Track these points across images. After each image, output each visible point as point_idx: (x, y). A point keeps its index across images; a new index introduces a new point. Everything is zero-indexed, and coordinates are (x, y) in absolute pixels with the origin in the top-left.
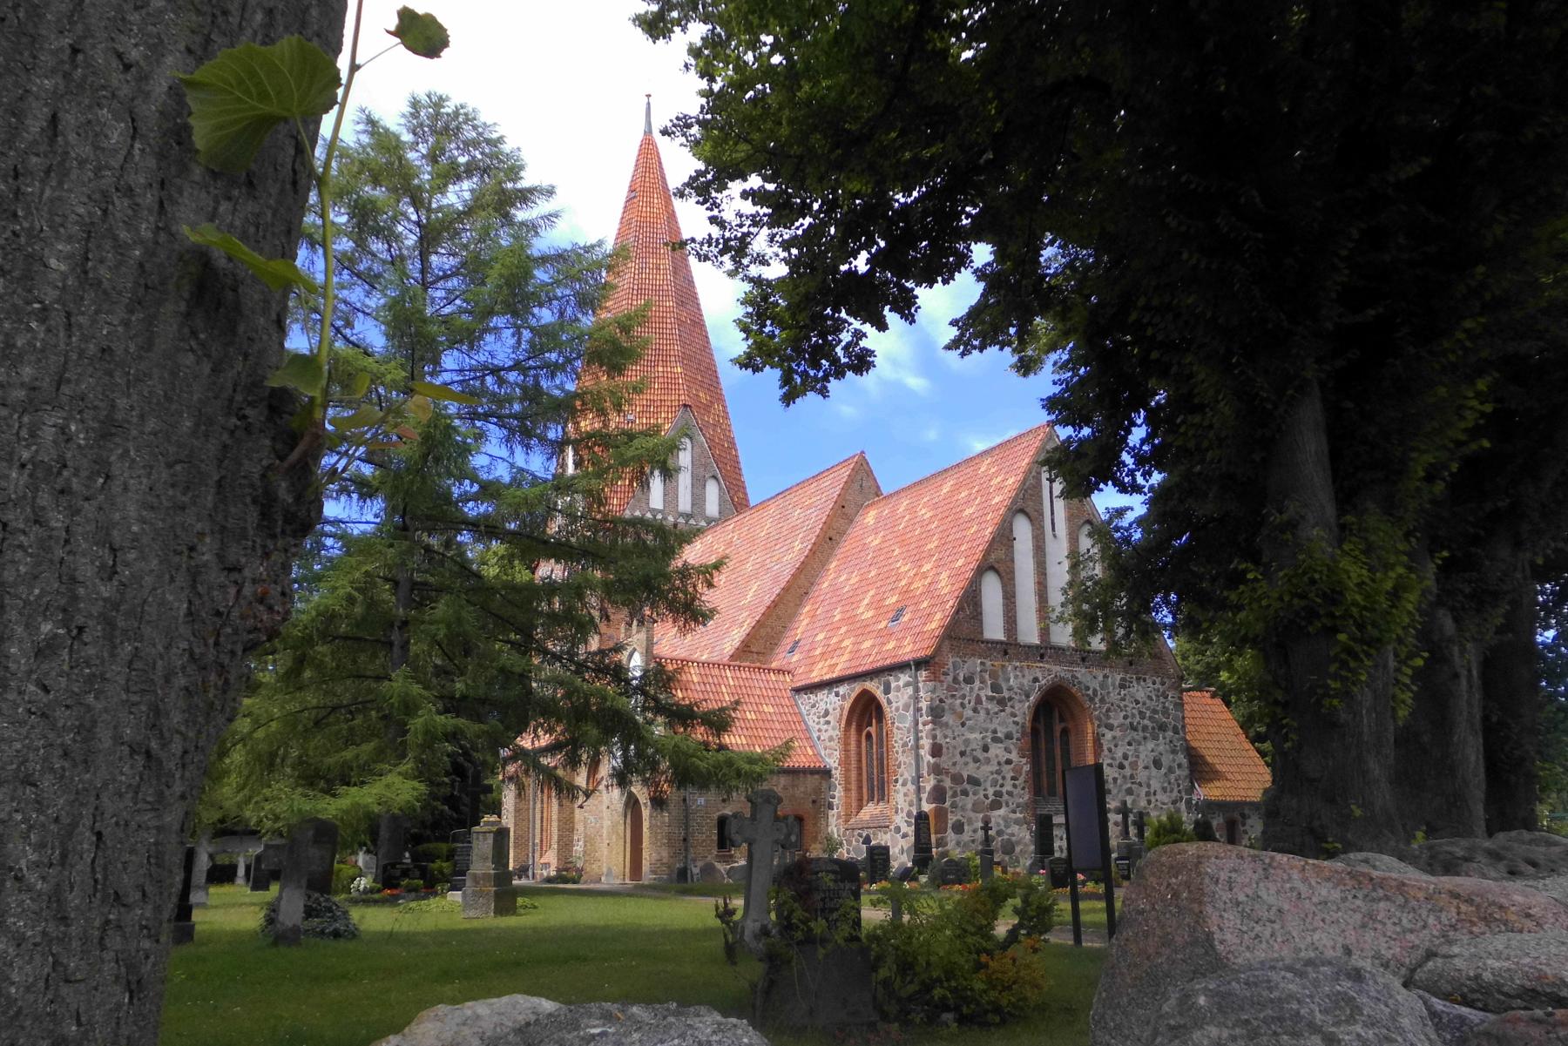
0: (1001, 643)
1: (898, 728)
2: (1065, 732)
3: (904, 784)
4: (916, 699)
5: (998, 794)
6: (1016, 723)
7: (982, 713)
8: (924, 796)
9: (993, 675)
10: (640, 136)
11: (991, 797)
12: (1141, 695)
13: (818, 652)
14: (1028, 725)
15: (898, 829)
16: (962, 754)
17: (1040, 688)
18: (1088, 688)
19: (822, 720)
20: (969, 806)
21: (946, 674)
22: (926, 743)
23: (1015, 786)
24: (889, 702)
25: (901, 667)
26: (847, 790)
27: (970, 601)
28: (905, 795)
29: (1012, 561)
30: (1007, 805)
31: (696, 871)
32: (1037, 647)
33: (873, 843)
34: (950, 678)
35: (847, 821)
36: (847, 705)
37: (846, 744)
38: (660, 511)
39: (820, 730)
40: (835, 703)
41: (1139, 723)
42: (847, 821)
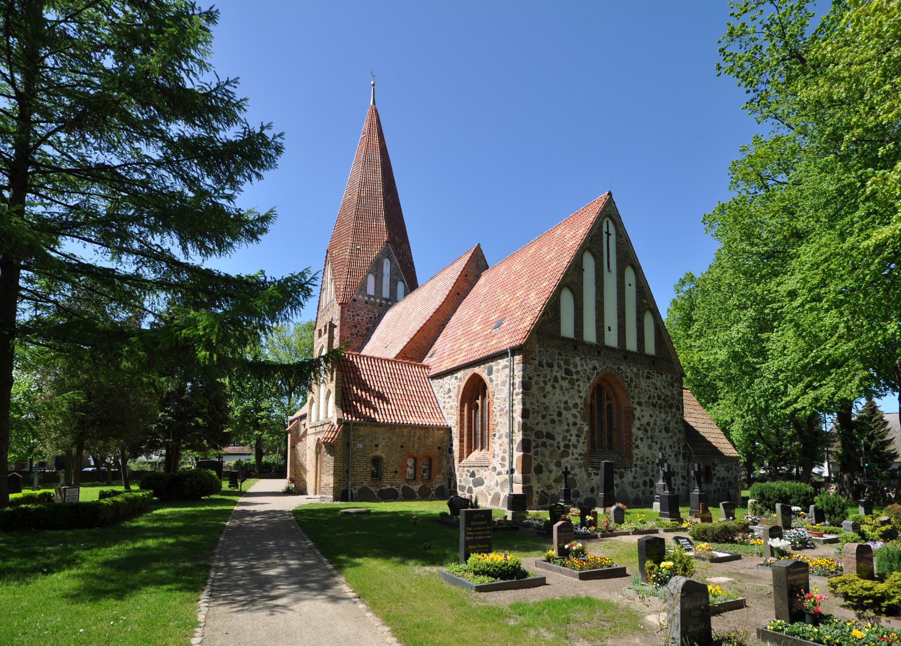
1: (497, 399)
3: (500, 438)
5: (567, 446)
8: (515, 446)
9: (567, 362)
11: (562, 449)
12: (659, 384)
13: (446, 355)
15: (494, 469)
16: (544, 417)
17: (598, 374)
18: (627, 377)
19: (446, 396)
20: (548, 453)
23: (578, 441)
24: (491, 380)
25: (500, 355)
27: (552, 309)
28: (501, 445)
29: (582, 284)
30: (573, 454)
33: (477, 477)
34: (536, 362)
36: (463, 385)
37: (462, 411)
38: (372, 296)
39: (445, 402)
40: (455, 384)
41: (657, 402)
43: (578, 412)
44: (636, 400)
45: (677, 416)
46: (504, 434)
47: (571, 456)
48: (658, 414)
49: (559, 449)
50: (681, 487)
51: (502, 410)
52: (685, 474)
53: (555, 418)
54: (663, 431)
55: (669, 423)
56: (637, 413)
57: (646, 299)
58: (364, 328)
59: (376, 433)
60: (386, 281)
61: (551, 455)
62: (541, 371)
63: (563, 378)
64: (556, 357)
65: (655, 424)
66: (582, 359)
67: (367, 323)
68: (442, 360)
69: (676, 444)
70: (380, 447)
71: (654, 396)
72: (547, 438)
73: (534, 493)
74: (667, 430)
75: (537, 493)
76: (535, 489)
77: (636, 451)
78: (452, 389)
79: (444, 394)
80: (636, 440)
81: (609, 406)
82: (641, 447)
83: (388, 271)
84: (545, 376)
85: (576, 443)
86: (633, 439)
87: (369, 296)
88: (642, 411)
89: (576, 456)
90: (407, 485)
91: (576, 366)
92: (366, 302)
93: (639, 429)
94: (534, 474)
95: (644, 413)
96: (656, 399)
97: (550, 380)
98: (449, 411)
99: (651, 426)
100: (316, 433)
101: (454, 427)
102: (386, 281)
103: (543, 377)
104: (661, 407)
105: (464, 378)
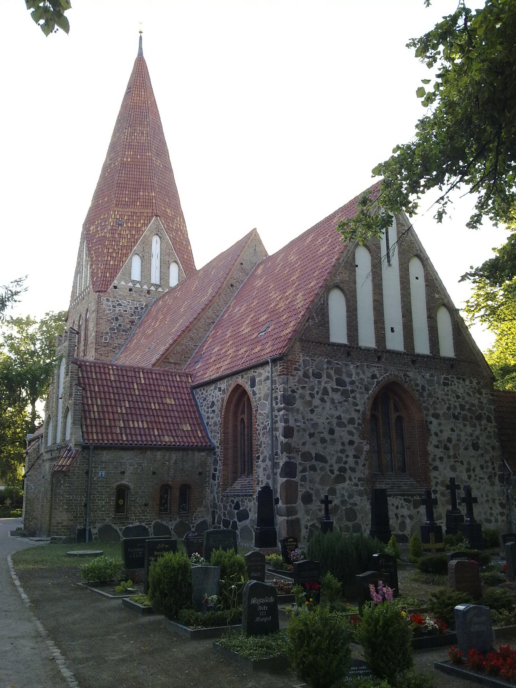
0: (345, 345)
1: (261, 414)
2: (399, 419)
3: (264, 461)
4: (273, 390)
5: (342, 470)
6: (358, 411)
7: (328, 404)
9: (338, 371)
10: (135, 55)
11: (336, 473)
12: (460, 392)
13: (212, 360)
14: (368, 413)
16: (311, 435)
17: (378, 383)
18: (417, 385)
19: (210, 410)
20: (318, 479)
21: (297, 369)
22: (281, 425)
23: (357, 463)
24: (254, 394)
26: (225, 464)
28: (265, 469)
30: (350, 479)
31: (95, 531)
32: (375, 350)
33: (241, 509)
34: (300, 373)
35: (224, 490)
36: (226, 397)
38: (138, 282)
39: (208, 418)
42: (224, 490)
43: (355, 428)
44: (432, 411)
45: (489, 429)
46: (268, 456)
47: (348, 482)
48: (461, 426)
49: (333, 473)
50: (500, 518)
51: (265, 428)
52: (504, 501)
53: (327, 436)
54: (471, 448)
55: (478, 438)
56: (434, 427)
57: (438, 292)
58: (127, 321)
59: (122, 458)
60: (155, 263)
61: (323, 482)
62: (306, 383)
63: (334, 390)
64: (325, 366)
65: (459, 440)
66: (357, 367)
67: (132, 315)
68: (207, 366)
69: (490, 464)
70: (126, 474)
71: (455, 407)
72: (316, 460)
73: (303, 527)
74: (476, 447)
75: (306, 527)
76: (303, 523)
77: (434, 474)
78: (215, 402)
79: (208, 408)
80: (434, 460)
81: (399, 419)
82: (441, 467)
83: (158, 250)
84: (312, 389)
85: (353, 465)
86: (430, 458)
87: (134, 282)
88: (440, 424)
89: (355, 481)
90: (159, 521)
91: (350, 375)
92: (130, 290)
93: (437, 447)
94: (302, 504)
95: (442, 427)
96: (459, 410)
97: (318, 393)
98: (213, 428)
99: (454, 442)
100: (52, 460)
101: (218, 447)
102: (155, 263)
103: (309, 389)
104: (465, 418)
105: (228, 389)
